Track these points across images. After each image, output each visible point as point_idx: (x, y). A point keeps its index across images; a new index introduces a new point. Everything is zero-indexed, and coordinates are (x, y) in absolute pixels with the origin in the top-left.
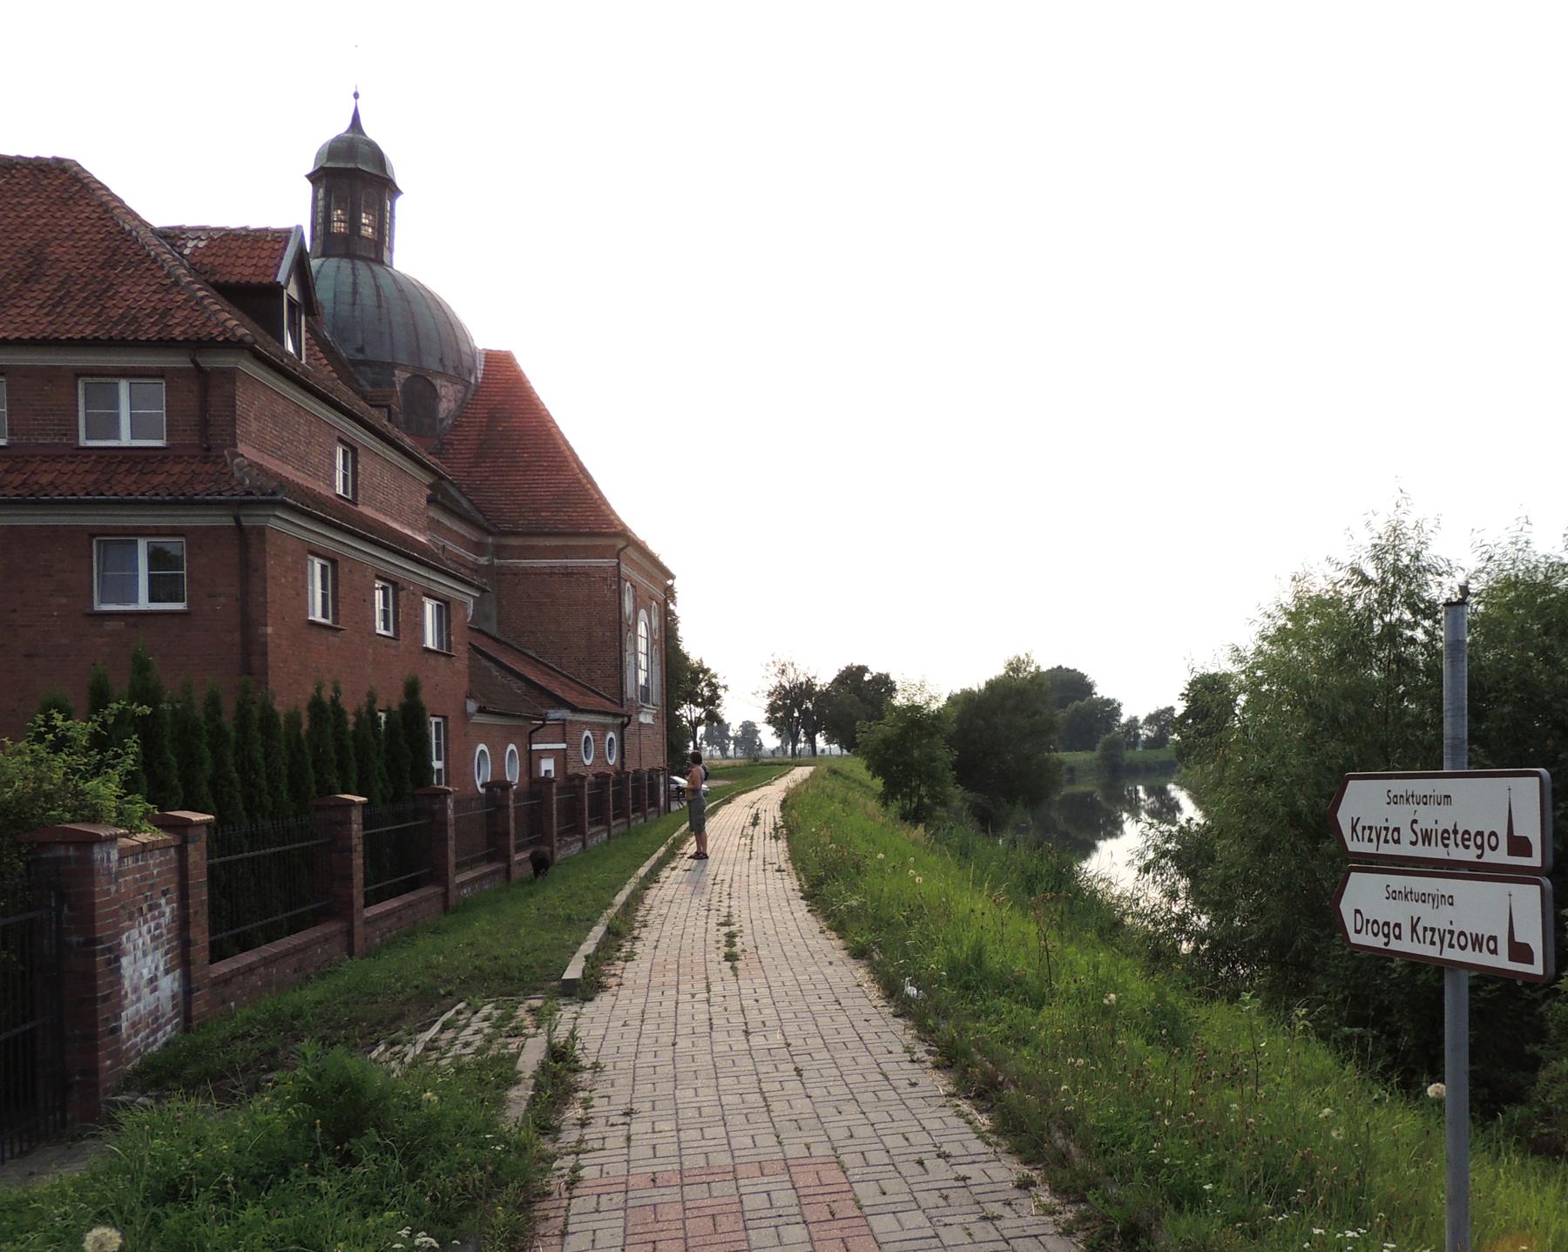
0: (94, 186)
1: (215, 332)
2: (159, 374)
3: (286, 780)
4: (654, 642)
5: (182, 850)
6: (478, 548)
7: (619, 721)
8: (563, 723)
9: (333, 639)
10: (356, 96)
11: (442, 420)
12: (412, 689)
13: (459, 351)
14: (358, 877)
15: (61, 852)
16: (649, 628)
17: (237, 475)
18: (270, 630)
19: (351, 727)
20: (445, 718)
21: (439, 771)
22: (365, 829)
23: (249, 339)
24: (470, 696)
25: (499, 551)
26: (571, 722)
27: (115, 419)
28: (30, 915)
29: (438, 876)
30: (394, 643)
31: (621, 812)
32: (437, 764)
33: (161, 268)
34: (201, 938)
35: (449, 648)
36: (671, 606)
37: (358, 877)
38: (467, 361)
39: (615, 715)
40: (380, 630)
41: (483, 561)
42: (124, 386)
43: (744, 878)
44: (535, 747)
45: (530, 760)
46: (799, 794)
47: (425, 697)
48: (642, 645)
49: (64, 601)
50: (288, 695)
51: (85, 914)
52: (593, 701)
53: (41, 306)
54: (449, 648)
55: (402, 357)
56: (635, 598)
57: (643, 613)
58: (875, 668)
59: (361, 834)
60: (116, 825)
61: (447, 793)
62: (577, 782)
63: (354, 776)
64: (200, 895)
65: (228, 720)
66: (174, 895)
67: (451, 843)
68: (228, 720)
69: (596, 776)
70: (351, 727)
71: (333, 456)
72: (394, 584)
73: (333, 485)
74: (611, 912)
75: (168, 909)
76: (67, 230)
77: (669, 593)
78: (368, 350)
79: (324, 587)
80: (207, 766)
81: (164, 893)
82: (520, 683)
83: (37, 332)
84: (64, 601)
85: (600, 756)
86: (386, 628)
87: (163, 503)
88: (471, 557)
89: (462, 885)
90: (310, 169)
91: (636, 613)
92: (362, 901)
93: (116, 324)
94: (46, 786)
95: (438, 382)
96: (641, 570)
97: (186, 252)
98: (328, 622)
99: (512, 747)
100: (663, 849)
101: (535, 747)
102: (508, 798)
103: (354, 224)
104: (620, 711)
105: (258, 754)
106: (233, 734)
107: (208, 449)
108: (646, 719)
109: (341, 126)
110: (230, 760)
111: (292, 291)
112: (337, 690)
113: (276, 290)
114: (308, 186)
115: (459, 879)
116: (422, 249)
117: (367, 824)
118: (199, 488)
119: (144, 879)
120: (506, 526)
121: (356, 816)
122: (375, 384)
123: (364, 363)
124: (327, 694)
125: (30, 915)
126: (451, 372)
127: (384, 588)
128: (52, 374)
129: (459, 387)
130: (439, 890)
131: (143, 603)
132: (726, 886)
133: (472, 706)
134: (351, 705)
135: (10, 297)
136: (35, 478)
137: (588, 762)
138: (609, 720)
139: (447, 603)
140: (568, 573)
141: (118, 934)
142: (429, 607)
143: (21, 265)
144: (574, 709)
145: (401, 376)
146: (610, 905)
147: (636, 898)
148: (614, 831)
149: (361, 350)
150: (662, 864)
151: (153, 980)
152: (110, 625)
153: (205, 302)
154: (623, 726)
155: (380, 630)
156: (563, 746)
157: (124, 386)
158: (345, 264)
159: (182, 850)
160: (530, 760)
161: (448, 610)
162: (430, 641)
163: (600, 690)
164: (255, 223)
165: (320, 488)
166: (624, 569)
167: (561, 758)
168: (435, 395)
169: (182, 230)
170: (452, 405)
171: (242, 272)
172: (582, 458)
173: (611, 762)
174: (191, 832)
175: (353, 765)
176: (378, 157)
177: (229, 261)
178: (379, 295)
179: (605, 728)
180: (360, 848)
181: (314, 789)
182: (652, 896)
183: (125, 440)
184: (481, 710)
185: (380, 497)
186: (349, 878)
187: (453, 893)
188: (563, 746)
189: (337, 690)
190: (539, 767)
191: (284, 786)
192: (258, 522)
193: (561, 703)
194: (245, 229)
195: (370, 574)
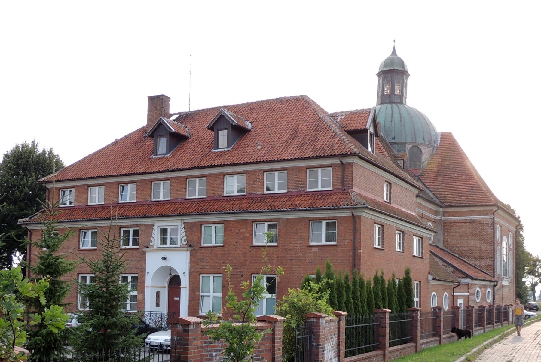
0: (312, 103)
1: (348, 150)
2: (330, 166)
3: (366, 303)
4: (510, 250)
5: (339, 322)
6: (436, 213)
7: (492, 284)
8: (468, 285)
9: (381, 253)
10: (394, 41)
11: (423, 162)
12: (407, 273)
13: (431, 134)
14: (387, 336)
15: (312, 320)
16: (508, 244)
17: (353, 198)
18: (361, 251)
19: (386, 286)
20: (420, 282)
21: (417, 302)
22: (390, 320)
23: (357, 152)
24: (430, 274)
25: (445, 214)
26: (471, 284)
27: (317, 181)
28: (304, 336)
29: (414, 340)
30: (402, 254)
31: (490, 322)
32: (416, 299)
33: (331, 129)
35: (422, 255)
36: (521, 233)
37: (387, 336)
38: (434, 138)
39: (491, 281)
40: (398, 249)
41: (438, 218)
43: (526, 348)
44: (455, 294)
45: (453, 299)
47: (411, 275)
48: (504, 251)
49: (301, 242)
50: (367, 275)
51: (318, 338)
52: (481, 275)
53: (297, 147)
54: (422, 255)
55: (409, 140)
57: (505, 238)
59: (389, 322)
60: (325, 314)
61: (418, 310)
62: (470, 309)
63: (387, 303)
64: (343, 336)
65: (351, 284)
66: (336, 335)
67: (419, 328)
68: (351, 284)
69: (479, 307)
70: (386, 286)
71: (383, 187)
72: (403, 232)
73: (383, 198)
74: (469, 354)
75: (335, 339)
76: (305, 120)
77: (519, 227)
78: (396, 138)
79: (379, 235)
80: (345, 298)
81: (334, 335)
82: (451, 268)
83: (296, 156)
84: (301, 242)
85: (484, 298)
86: (400, 248)
88: (433, 216)
89: (423, 344)
90: (377, 72)
91: (502, 237)
92: (388, 345)
93: (318, 151)
94: (308, 302)
95: (422, 148)
96: (504, 218)
97: (338, 121)
98: (380, 247)
99: (434, 293)
100: (498, 336)
102: (440, 313)
103: (392, 90)
104: (493, 279)
105: (358, 295)
106: (352, 288)
107: (344, 190)
108: (505, 283)
109: (388, 54)
110: (351, 296)
111: (371, 130)
112: (382, 273)
113: (366, 131)
114: (377, 78)
115: (422, 341)
116: (418, 97)
117: (391, 319)
118: (342, 203)
119: (330, 330)
120: (447, 204)
121: (387, 316)
122: (399, 151)
123: (395, 143)
124: (379, 274)
125: (304, 336)
126: (427, 143)
127: (399, 234)
128: (300, 169)
129: (431, 149)
130: (414, 344)
131: (324, 243)
132: (516, 351)
133: (430, 277)
134: (387, 278)
135: (289, 145)
136: (294, 202)
137: (478, 301)
138: (488, 283)
139: (422, 238)
140: (472, 222)
141: (324, 344)
142: (416, 240)
143: (292, 134)
144: (472, 279)
145: (408, 147)
146: (469, 352)
147: (480, 351)
148: (486, 330)
149: (394, 138)
150: (496, 341)
151: (331, 359)
152: (314, 250)
153: (345, 140)
154: (494, 286)
155: (398, 249)
156: (468, 294)
158: (389, 106)
159: (339, 322)
160: (453, 299)
161: (422, 241)
162: (415, 253)
163: (485, 270)
164: (359, 108)
165: (379, 199)
166: (496, 219)
169: (337, 113)
171: (354, 126)
172: (479, 173)
173: (489, 301)
174: (341, 317)
175: (387, 299)
176: (402, 63)
177: (352, 122)
178: (401, 117)
179: (486, 287)
180: (388, 327)
181: (374, 306)
182: (486, 351)
183: (320, 189)
184: (434, 279)
185: (399, 200)
186: (384, 336)
187: (419, 347)
188: (468, 294)
189: (382, 273)
190: (457, 301)
191: (365, 305)
192: (359, 214)
193: (467, 276)
194: (357, 110)
195: (395, 229)
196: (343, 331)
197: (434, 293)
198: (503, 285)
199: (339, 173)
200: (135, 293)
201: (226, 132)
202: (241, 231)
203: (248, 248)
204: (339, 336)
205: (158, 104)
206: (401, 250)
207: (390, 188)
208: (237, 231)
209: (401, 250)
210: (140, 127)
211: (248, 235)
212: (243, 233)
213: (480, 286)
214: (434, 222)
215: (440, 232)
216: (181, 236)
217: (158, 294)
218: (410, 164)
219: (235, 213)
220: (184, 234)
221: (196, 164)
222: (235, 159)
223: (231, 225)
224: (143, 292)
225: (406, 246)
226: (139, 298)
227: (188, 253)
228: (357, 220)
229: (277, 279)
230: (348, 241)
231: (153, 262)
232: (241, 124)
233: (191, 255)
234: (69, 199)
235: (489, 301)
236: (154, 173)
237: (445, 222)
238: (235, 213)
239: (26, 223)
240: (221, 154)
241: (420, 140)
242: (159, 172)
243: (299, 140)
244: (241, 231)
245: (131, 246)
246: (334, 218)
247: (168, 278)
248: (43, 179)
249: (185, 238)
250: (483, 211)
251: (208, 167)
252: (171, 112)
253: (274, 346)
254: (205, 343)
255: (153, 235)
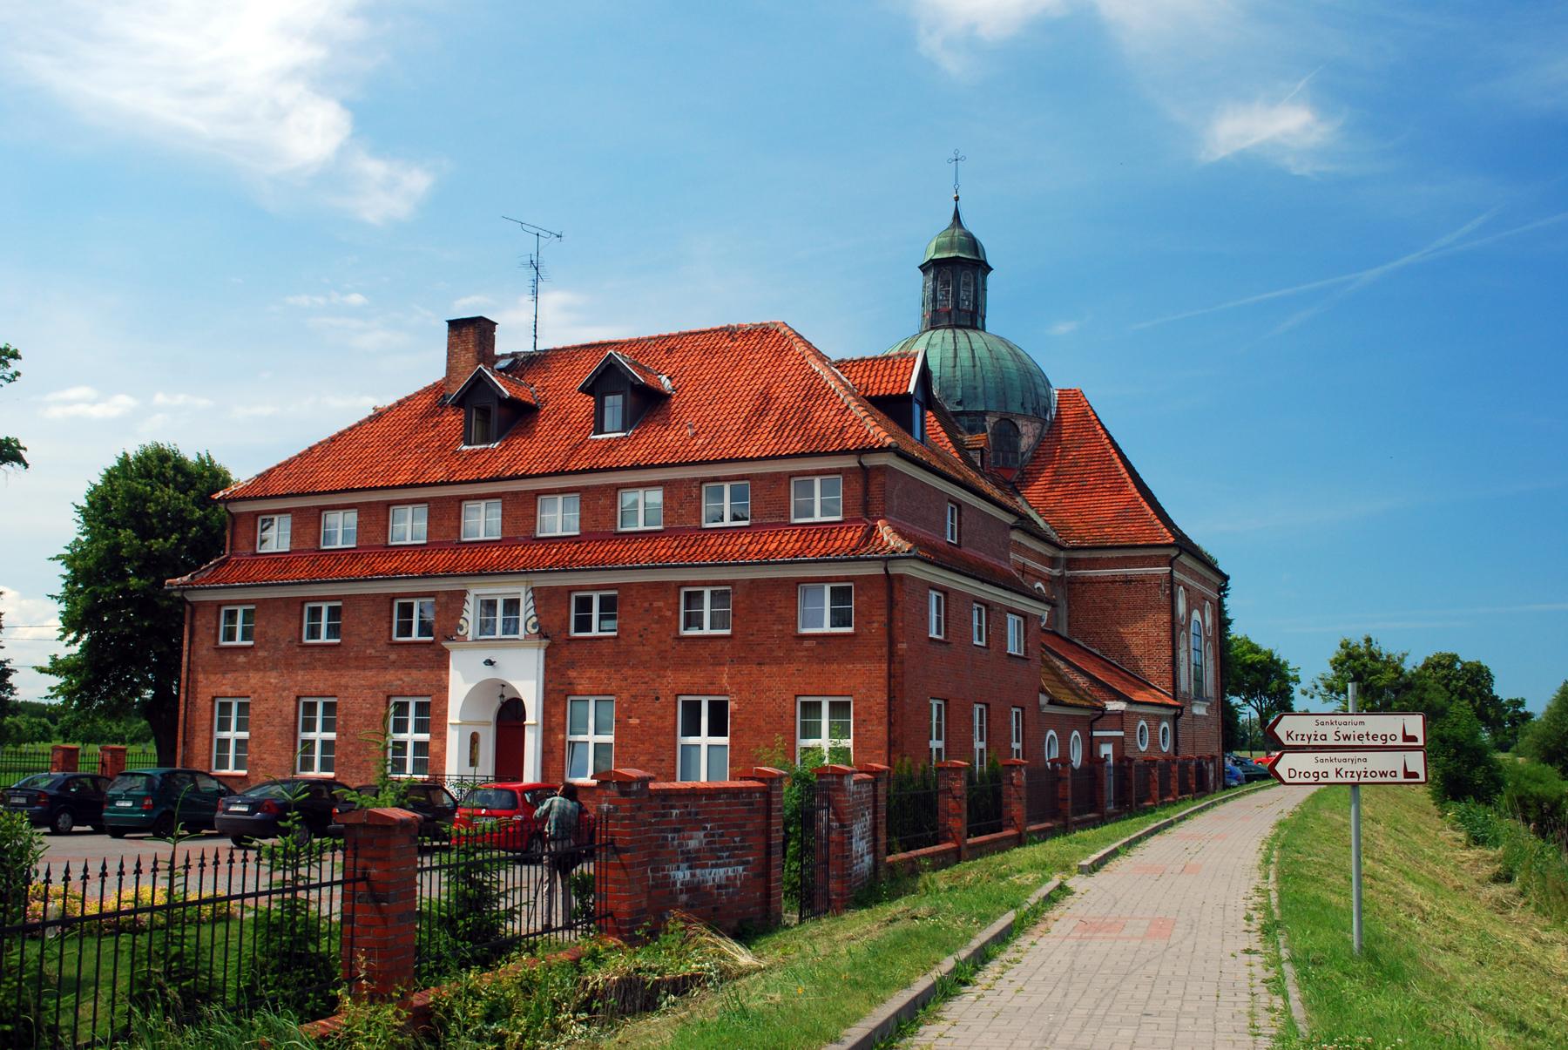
6: (1052, 562)
7: (1172, 712)
13: (1037, 394)
25: (1071, 563)
32: (1016, 746)
34: (883, 838)
41: (1056, 572)
42: (817, 481)
44: (1096, 734)
45: (1091, 746)
46: (440, 668)
56: (1188, 600)
58: (1467, 656)
73: (944, 535)
79: (938, 612)
85: (1154, 743)
87: (841, 561)
88: (1046, 570)
91: (1189, 612)
95: (1019, 423)
96: (1192, 573)
98: (941, 637)
99: (1076, 733)
101: (1096, 734)
108: (1199, 710)
138: (1163, 711)
140: (1127, 581)
149: (959, 403)
152: (807, 644)
154: (1176, 717)
157: (817, 481)
158: (949, 334)
160: (1091, 746)
166: (1176, 574)
167: (1118, 743)
168: (1018, 433)
170: (1031, 441)
171: (886, 388)
173: (1165, 749)
179: (1159, 719)
184: (1052, 702)
196: (882, 803)
197: (1051, 732)
198: (1194, 716)
199: (857, 487)
200: (425, 737)
201: (619, 399)
202: (656, 604)
203: (670, 640)
204: (875, 813)
205: (472, 333)
206: (983, 644)
207: (959, 515)
208: (646, 605)
209: (983, 644)
210: (429, 383)
211: (669, 614)
212: (660, 609)
213: (1147, 717)
214: (1049, 581)
215: (1063, 604)
216: (526, 612)
217: (474, 739)
218: (996, 457)
219: (642, 568)
220: (532, 612)
221: (557, 465)
222: (640, 454)
223: (633, 592)
224: (441, 736)
225: (997, 635)
226: (434, 748)
227: (542, 652)
228: (897, 585)
229: (732, 706)
230: (877, 625)
231: (462, 680)
232: (651, 382)
233: (547, 656)
234: (277, 538)
235: (1165, 749)
236: (467, 482)
237: (1072, 581)
238: (642, 568)
239: (183, 589)
240: (611, 445)
241: (1015, 408)
242: (479, 481)
243: (773, 417)
244: (656, 604)
245: (415, 636)
246: (847, 579)
247: (497, 704)
248: (221, 493)
249: (534, 619)
250: (1150, 557)
251: (584, 472)
252: (498, 351)
253: (769, 825)
254: (655, 816)
255: (465, 615)
